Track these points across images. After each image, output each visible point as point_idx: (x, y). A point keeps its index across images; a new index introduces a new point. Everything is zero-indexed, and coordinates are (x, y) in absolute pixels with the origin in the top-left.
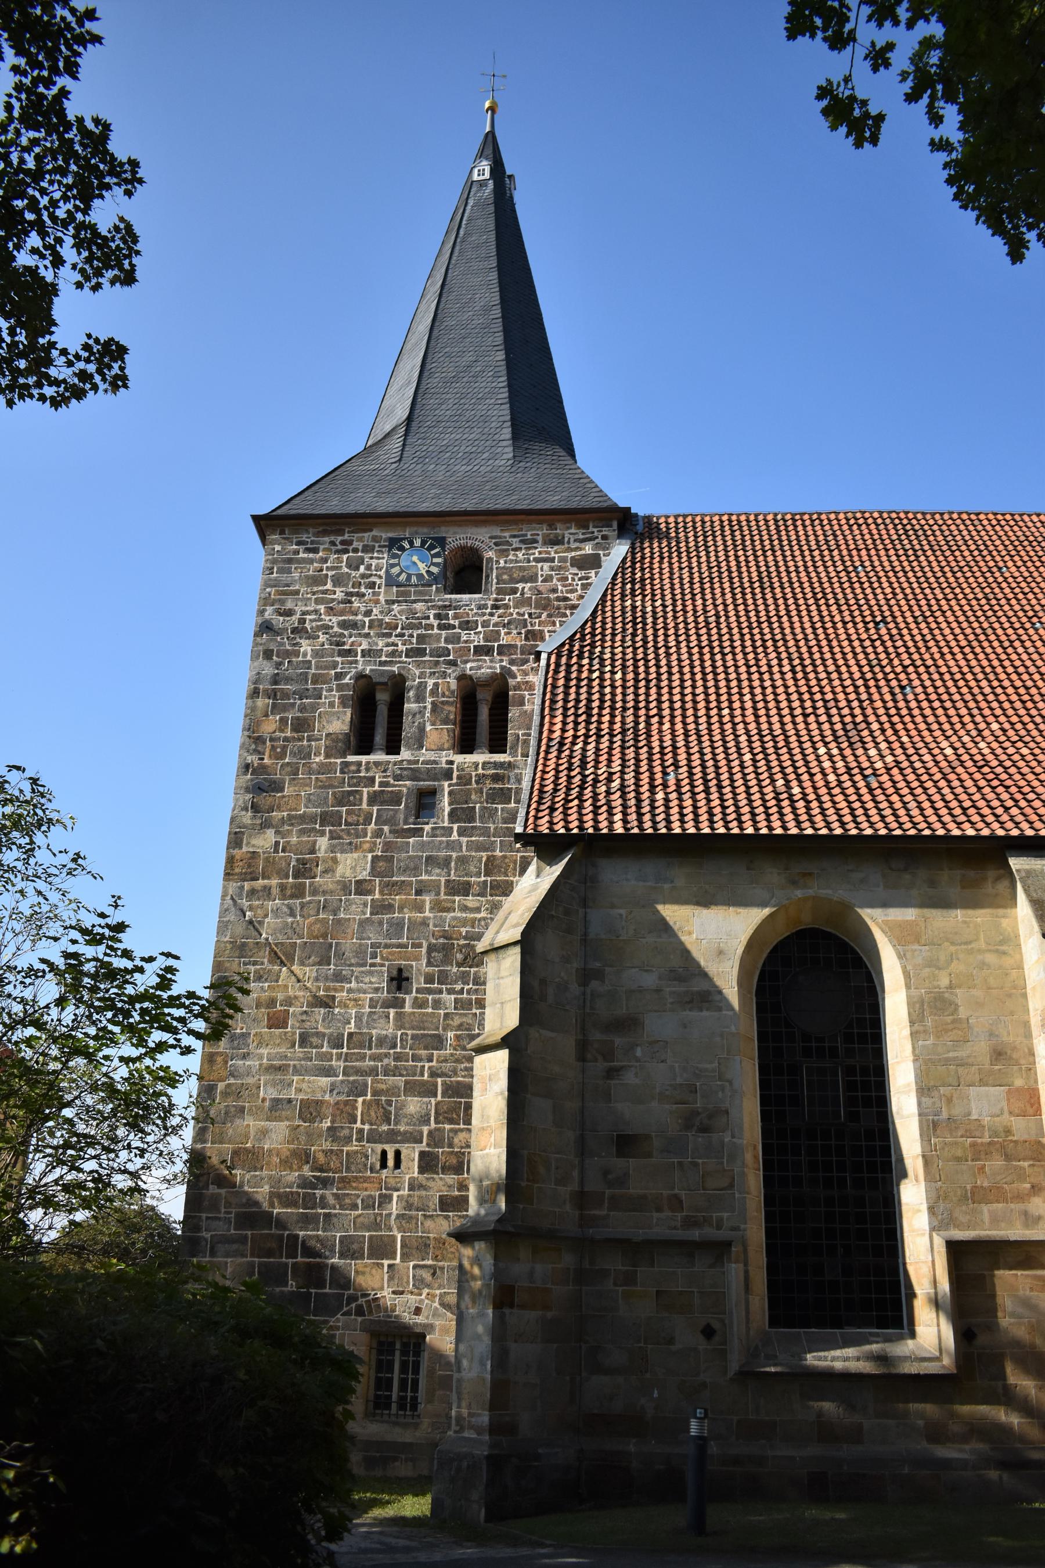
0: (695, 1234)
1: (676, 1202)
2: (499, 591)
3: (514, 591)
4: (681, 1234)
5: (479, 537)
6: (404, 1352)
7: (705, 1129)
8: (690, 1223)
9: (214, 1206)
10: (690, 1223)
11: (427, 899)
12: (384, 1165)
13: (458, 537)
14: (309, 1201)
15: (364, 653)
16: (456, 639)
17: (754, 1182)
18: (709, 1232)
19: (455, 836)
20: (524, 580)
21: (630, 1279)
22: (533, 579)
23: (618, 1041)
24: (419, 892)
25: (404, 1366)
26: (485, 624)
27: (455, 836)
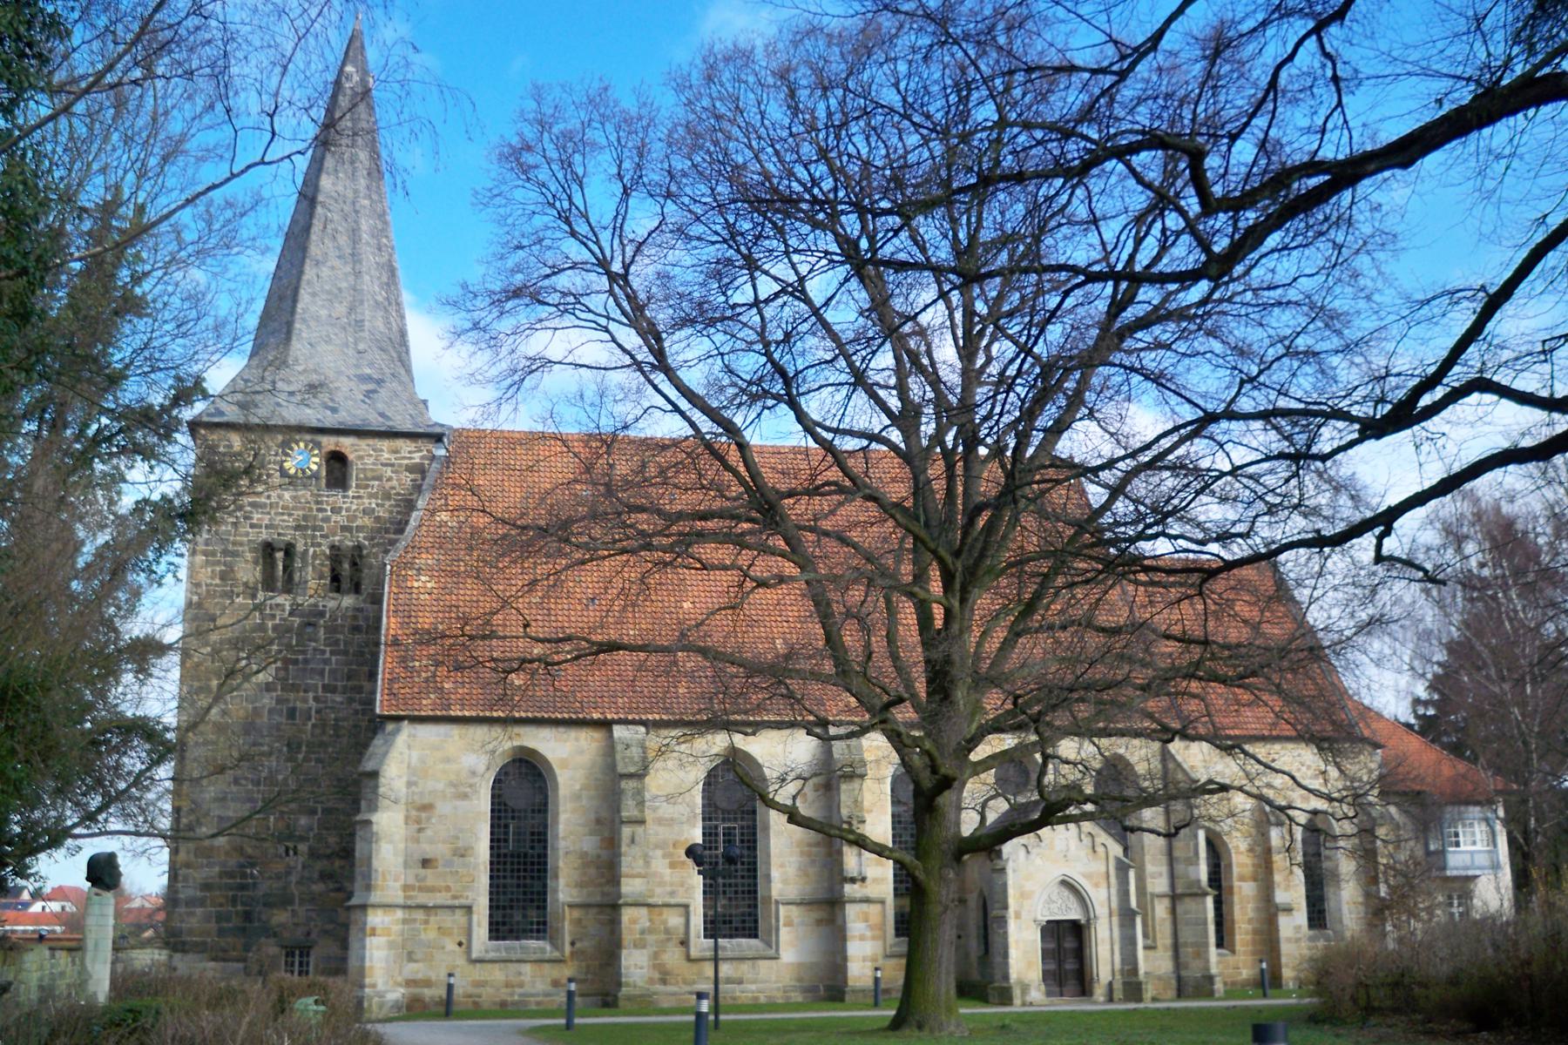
0: (457, 902)
1: (448, 889)
2: (358, 486)
3: (367, 486)
4: (449, 902)
5: (346, 444)
6: (301, 955)
7: (462, 856)
8: (455, 897)
9: (186, 879)
10: (455, 897)
11: (311, 695)
12: (287, 854)
13: (329, 443)
14: (244, 876)
15: (267, 527)
16: (326, 520)
17: (484, 880)
18: (463, 901)
19: (327, 655)
20: (374, 478)
21: (426, 922)
22: (379, 478)
23: (423, 815)
24: (306, 691)
25: (301, 964)
26: (348, 510)
27: (327, 655)
